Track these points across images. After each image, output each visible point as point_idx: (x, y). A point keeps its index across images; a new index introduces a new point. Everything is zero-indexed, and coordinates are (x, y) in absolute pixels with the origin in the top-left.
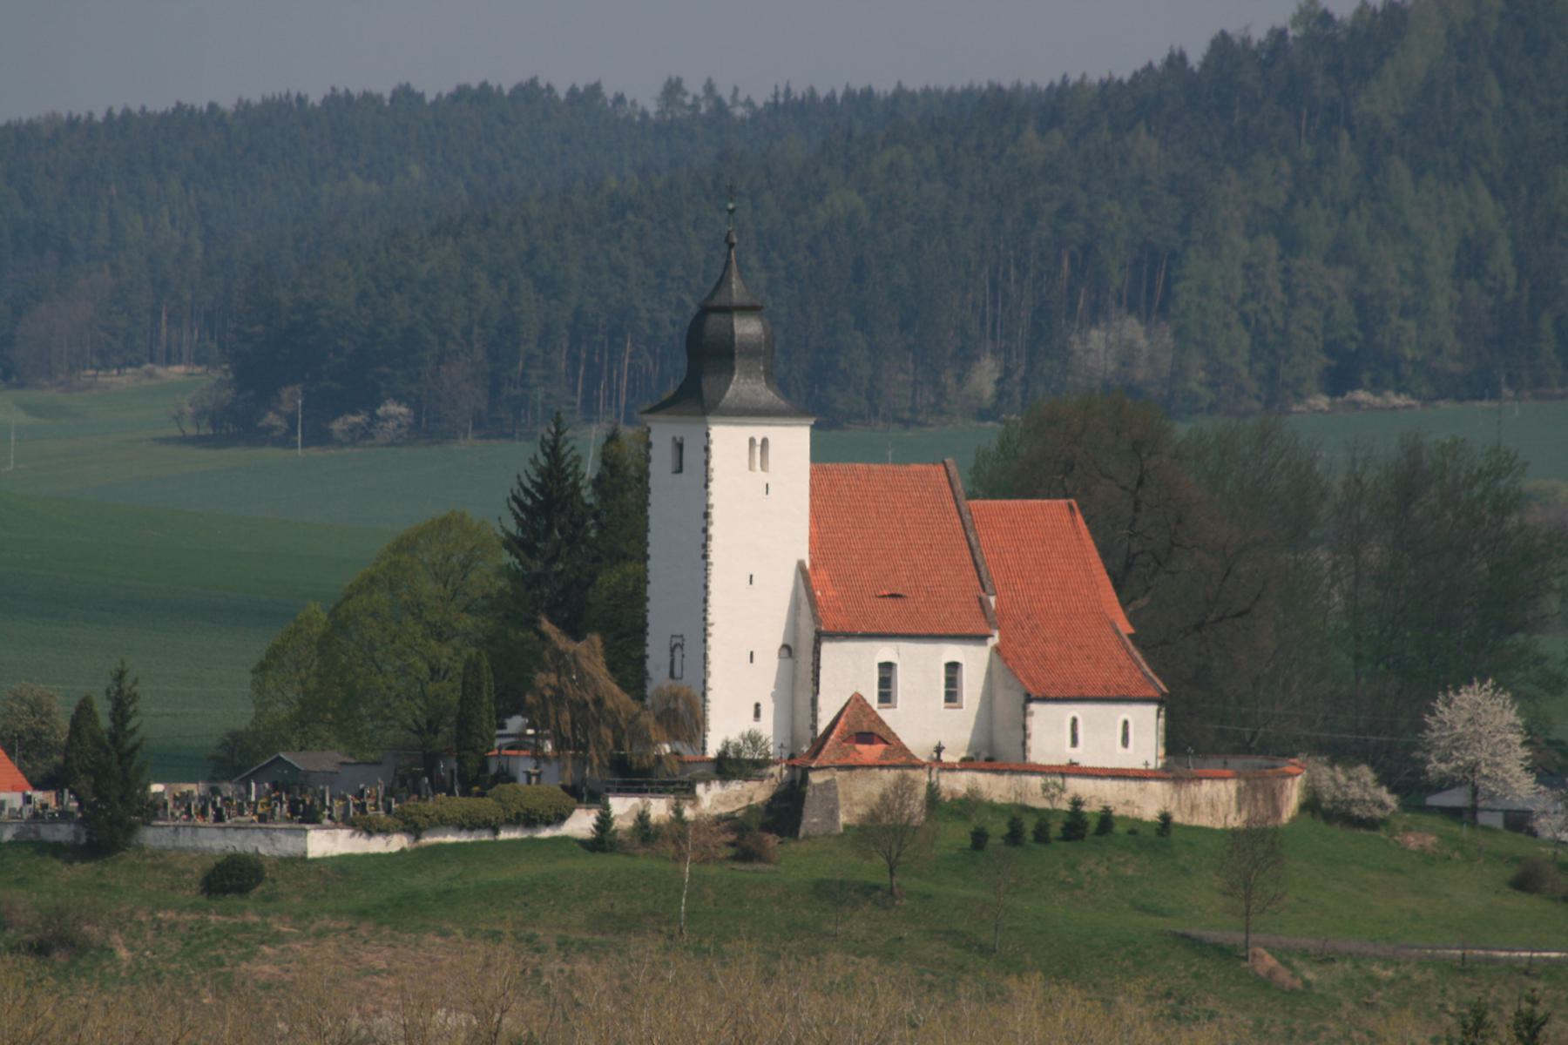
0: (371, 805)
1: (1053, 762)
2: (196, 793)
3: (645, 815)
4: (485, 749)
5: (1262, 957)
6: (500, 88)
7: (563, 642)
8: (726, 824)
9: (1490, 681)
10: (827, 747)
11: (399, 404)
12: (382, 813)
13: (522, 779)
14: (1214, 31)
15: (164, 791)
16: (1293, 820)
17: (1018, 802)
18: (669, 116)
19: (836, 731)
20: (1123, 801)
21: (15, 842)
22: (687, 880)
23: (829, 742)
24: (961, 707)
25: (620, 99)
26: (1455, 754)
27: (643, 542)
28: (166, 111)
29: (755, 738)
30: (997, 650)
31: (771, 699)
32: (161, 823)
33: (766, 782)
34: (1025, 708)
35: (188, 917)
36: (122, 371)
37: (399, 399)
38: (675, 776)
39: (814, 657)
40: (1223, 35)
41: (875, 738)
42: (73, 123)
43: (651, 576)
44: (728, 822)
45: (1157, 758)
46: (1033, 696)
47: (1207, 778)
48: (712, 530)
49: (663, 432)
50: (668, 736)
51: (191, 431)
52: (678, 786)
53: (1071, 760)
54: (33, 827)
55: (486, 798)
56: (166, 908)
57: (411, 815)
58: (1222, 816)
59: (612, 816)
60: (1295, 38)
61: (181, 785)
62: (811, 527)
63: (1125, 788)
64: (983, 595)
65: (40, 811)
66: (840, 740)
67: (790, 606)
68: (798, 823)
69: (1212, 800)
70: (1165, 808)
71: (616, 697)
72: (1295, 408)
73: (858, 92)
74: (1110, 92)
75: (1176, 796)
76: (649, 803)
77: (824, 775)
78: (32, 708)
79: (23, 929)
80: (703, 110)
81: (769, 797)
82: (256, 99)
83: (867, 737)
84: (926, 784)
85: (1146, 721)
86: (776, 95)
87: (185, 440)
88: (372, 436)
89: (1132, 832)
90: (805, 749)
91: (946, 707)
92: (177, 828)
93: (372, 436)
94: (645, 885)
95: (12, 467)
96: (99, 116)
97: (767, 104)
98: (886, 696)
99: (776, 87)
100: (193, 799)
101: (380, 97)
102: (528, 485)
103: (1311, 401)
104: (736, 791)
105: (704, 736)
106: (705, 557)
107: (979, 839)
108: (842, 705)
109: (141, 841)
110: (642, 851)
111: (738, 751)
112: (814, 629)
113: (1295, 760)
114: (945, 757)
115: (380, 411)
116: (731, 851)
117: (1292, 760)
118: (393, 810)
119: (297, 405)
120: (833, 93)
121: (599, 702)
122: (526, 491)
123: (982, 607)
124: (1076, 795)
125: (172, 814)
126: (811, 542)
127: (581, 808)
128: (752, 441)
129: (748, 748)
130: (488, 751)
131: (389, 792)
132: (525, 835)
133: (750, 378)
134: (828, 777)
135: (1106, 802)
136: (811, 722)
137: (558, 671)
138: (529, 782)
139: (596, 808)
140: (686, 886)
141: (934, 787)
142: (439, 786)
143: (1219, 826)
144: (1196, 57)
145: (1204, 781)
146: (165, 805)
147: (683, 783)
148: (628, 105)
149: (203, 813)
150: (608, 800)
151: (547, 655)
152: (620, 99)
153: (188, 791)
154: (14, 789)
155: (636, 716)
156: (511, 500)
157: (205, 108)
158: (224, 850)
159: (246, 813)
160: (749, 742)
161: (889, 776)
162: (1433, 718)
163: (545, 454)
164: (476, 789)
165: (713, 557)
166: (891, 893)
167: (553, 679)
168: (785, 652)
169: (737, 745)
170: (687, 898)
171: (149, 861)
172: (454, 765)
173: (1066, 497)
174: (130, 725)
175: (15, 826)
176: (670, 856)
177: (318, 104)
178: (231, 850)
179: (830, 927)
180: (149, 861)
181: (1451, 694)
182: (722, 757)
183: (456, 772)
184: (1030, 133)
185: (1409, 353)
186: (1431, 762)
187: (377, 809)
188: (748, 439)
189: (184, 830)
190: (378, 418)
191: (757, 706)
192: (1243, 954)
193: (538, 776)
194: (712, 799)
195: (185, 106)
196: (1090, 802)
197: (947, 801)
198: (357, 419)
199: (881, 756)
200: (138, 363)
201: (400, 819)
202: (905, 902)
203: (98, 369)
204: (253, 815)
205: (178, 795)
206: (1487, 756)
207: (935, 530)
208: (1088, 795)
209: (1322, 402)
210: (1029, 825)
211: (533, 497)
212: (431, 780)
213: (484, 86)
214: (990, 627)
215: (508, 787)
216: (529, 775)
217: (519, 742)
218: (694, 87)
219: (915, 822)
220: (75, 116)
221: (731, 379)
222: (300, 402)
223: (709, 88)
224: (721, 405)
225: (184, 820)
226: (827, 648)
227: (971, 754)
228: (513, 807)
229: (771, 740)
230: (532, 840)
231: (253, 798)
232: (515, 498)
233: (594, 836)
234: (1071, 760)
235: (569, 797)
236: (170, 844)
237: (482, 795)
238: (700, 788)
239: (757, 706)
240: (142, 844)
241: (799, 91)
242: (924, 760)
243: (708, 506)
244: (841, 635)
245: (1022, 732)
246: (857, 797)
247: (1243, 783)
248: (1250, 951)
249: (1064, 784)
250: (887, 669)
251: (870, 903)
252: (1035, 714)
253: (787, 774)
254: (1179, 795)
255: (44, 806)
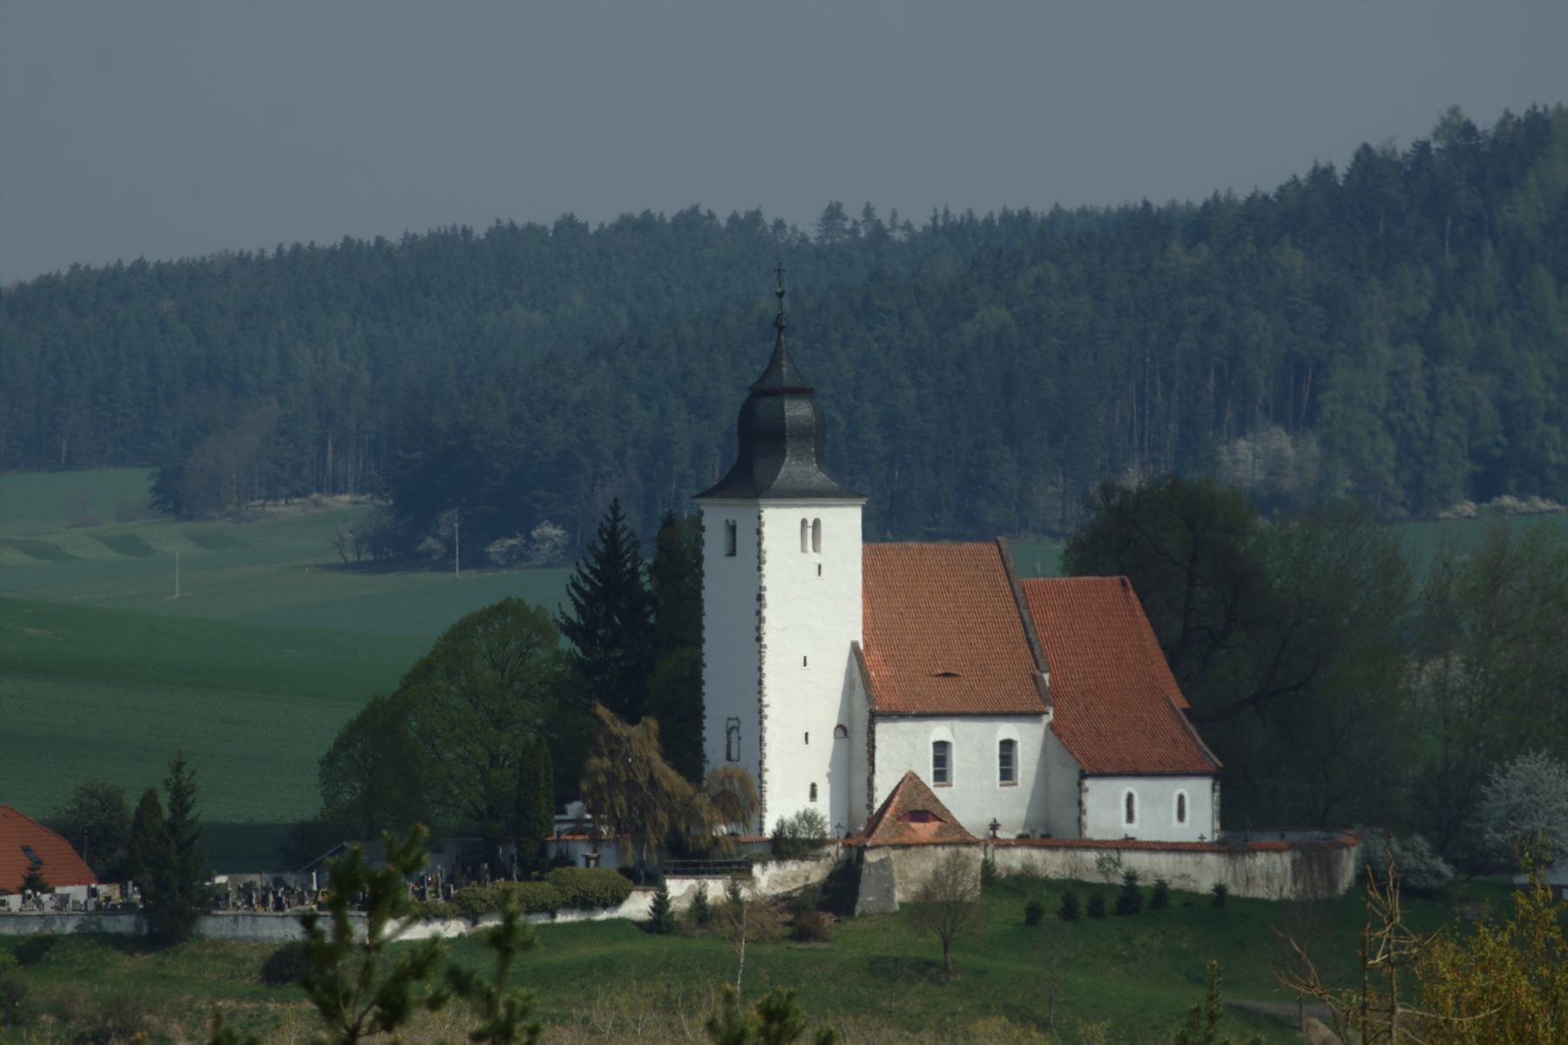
0: (430, 892)
1: (1110, 837)
2: (259, 885)
3: (702, 896)
4: (544, 834)
5: (1316, 1028)
6: (662, 215)
7: (619, 728)
8: (783, 904)
9: (1545, 751)
10: (881, 826)
11: (555, 527)
12: (441, 900)
13: (581, 862)
14: (1356, 145)
15: (227, 882)
16: (1349, 891)
17: (1074, 877)
18: (828, 242)
19: (891, 810)
20: (1179, 875)
21: (78, 934)
22: (742, 961)
23: (884, 821)
24: (1015, 784)
25: (779, 225)
26: (1512, 823)
27: (700, 627)
28: (335, 246)
29: (810, 817)
30: (1051, 726)
31: (827, 779)
32: (220, 912)
33: (822, 861)
34: (1080, 784)
35: (247, 1005)
36: (289, 501)
37: (555, 520)
38: (731, 856)
39: (868, 736)
40: (1366, 148)
41: (930, 816)
42: (244, 260)
43: (706, 659)
44: (784, 902)
45: (1213, 831)
46: (1087, 772)
47: (1262, 850)
48: (766, 613)
49: (715, 517)
50: (723, 817)
51: (352, 557)
52: (734, 867)
53: (1126, 835)
54: (94, 918)
55: (543, 882)
56: (227, 996)
57: (468, 899)
58: (1277, 887)
59: (669, 898)
60: (1438, 150)
61: (244, 876)
62: (865, 608)
63: (1180, 862)
64: (1037, 672)
65: (104, 904)
66: (894, 818)
67: (845, 686)
68: (854, 902)
69: (1268, 872)
70: (1220, 881)
71: (671, 779)
72: (1442, 515)
73: (1016, 213)
74: (1256, 207)
75: (1231, 868)
76: (705, 885)
77: (878, 854)
78: (102, 803)
79: (84, 1021)
80: (863, 234)
81: (825, 877)
82: (423, 232)
83: (922, 816)
84: (981, 861)
85: (1200, 795)
86: (934, 219)
87: (346, 567)
88: (528, 559)
89: (1187, 905)
90: (862, 829)
91: (1001, 785)
92: (236, 917)
93: (528, 559)
94: (702, 966)
95: (178, 595)
96: (271, 252)
97: (925, 228)
98: (941, 775)
99: (935, 210)
100: (257, 890)
101: (544, 228)
102: (586, 571)
103: (1458, 507)
104: (791, 871)
105: (761, 817)
106: (759, 639)
107: (1034, 915)
108: (895, 784)
109: (201, 931)
110: (698, 931)
111: (794, 830)
112: (868, 709)
113: (1351, 832)
114: (1000, 834)
115: (535, 534)
116: (788, 930)
117: (1348, 832)
118: (452, 896)
119: (454, 528)
120: (991, 215)
121: (653, 782)
122: (585, 578)
123: (1036, 683)
124: (1130, 869)
125: (234, 904)
126: (865, 623)
127: (638, 890)
128: (804, 522)
129: (804, 828)
130: (547, 837)
131: (450, 879)
132: (583, 918)
133: (802, 460)
134: (883, 856)
135: (1161, 875)
136: (867, 802)
137: (612, 754)
138: (588, 865)
139: (654, 890)
140: (742, 966)
141: (989, 864)
142: (499, 871)
143: (1274, 897)
144: (1342, 168)
145: (1259, 854)
146: (227, 897)
147: (739, 863)
148: (789, 231)
149: (264, 902)
150: (665, 882)
151: (601, 740)
152: (779, 225)
153: (251, 882)
154: (79, 883)
155: (692, 798)
156: (570, 586)
157: (372, 244)
158: (283, 939)
159: (307, 902)
160: (804, 822)
161: (942, 853)
162: (1489, 789)
163: (604, 541)
164: (535, 873)
165: (766, 640)
166: (945, 969)
167: (606, 763)
168: (841, 733)
169: (793, 824)
170: (743, 977)
171: (209, 951)
172: (514, 850)
173: (1120, 573)
174: (190, 815)
175: (77, 918)
176: (727, 936)
177: (483, 237)
178: (290, 938)
179: (885, 1004)
180: (209, 951)
181: (1507, 763)
182: (778, 836)
183: (516, 857)
184: (1176, 247)
185: (1553, 458)
186: (1488, 833)
187: (437, 896)
188: (800, 521)
189: (244, 919)
190: (534, 540)
191: (813, 786)
192: (1298, 1024)
193: (597, 859)
194: (768, 879)
195: (353, 241)
196: (1146, 876)
197: (1003, 877)
198: (512, 542)
199: (936, 833)
200: (304, 493)
201: (458, 904)
202: (959, 977)
203: (267, 499)
204: (314, 903)
205: (241, 886)
206: (1543, 825)
207: (1057, 634)
208: (1143, 869)
209: (1469, 508)
210: (1083, 901)
211: (592, 584)
212: (491, 866)
213: (647, 215)
214: (1045, 705)
215: (566, 870)
216: (588, 859)
217: (578, 827)
218: (853, 211)
219: (968, 899)
220: (246, 252)
221: (783, 461)
222: (457, 526)
223: (868, 212)
224: (773, 486)
225: (245, 909)
226: (883, 730)
227: (1027, 832)
228: (569, 890)
229: (827, 819)
230: (589, 923)
231: (315, 887)
232: (575, 585)
233: (651, 918)
234: (1126, 835)
235: (626, 879)
236: (230, 934)
237: (539, 879)
238: (757, 870)
239: (813, 786)
240: (203, 935)
241: (957, 213)
242: (980, 837)
243: (761, 588)
244: (894, 715)
245: (1078, 809)
246: (912, 875)
247: (1298, 855)
248: (1304, 1023)
249: (1119, 859)
250: (941, 749)
251: (925, 979)
252: (1090, 790)
253: (843, 855)
254: (1234, 868)
255: (108, 899)
